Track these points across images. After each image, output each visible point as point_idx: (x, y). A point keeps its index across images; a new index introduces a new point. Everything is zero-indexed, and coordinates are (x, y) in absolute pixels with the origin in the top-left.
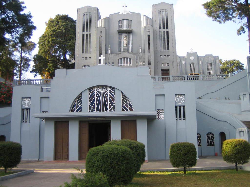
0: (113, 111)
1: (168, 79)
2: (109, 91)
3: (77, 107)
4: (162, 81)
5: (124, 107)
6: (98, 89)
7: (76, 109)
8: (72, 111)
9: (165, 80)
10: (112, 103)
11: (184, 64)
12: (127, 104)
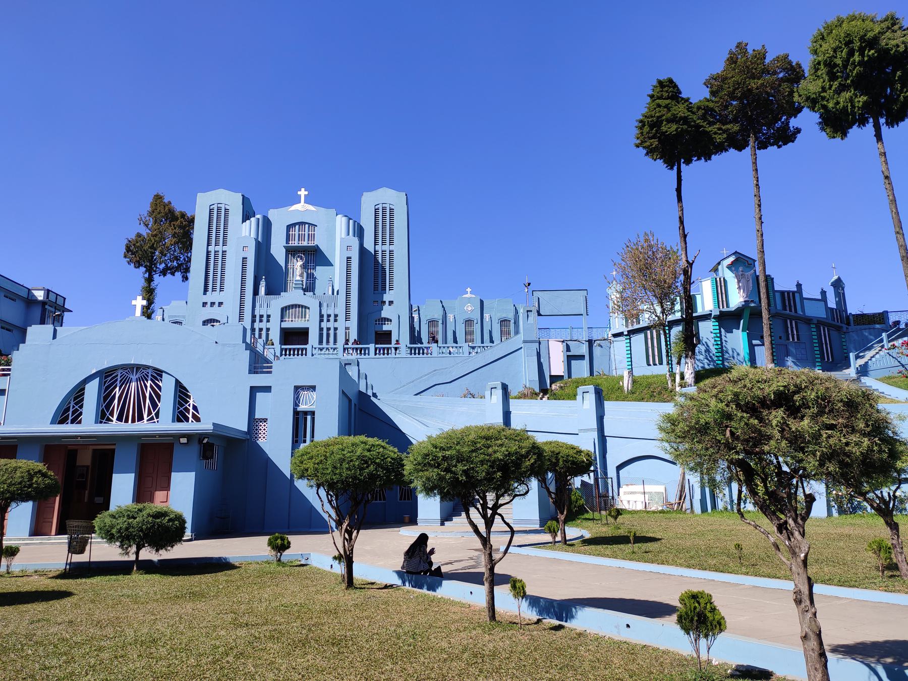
0: (155, 422)
1: (365, 351)
2: (150, 377)
3: (73, 413)
4: (409, 356)
5: (181, 412)
6: (126, 373)
7: (70, 418)
8: (62, 422)
9: (413, 354)
10: (155, 405)
11: (487, 320)
12: (189, 405)
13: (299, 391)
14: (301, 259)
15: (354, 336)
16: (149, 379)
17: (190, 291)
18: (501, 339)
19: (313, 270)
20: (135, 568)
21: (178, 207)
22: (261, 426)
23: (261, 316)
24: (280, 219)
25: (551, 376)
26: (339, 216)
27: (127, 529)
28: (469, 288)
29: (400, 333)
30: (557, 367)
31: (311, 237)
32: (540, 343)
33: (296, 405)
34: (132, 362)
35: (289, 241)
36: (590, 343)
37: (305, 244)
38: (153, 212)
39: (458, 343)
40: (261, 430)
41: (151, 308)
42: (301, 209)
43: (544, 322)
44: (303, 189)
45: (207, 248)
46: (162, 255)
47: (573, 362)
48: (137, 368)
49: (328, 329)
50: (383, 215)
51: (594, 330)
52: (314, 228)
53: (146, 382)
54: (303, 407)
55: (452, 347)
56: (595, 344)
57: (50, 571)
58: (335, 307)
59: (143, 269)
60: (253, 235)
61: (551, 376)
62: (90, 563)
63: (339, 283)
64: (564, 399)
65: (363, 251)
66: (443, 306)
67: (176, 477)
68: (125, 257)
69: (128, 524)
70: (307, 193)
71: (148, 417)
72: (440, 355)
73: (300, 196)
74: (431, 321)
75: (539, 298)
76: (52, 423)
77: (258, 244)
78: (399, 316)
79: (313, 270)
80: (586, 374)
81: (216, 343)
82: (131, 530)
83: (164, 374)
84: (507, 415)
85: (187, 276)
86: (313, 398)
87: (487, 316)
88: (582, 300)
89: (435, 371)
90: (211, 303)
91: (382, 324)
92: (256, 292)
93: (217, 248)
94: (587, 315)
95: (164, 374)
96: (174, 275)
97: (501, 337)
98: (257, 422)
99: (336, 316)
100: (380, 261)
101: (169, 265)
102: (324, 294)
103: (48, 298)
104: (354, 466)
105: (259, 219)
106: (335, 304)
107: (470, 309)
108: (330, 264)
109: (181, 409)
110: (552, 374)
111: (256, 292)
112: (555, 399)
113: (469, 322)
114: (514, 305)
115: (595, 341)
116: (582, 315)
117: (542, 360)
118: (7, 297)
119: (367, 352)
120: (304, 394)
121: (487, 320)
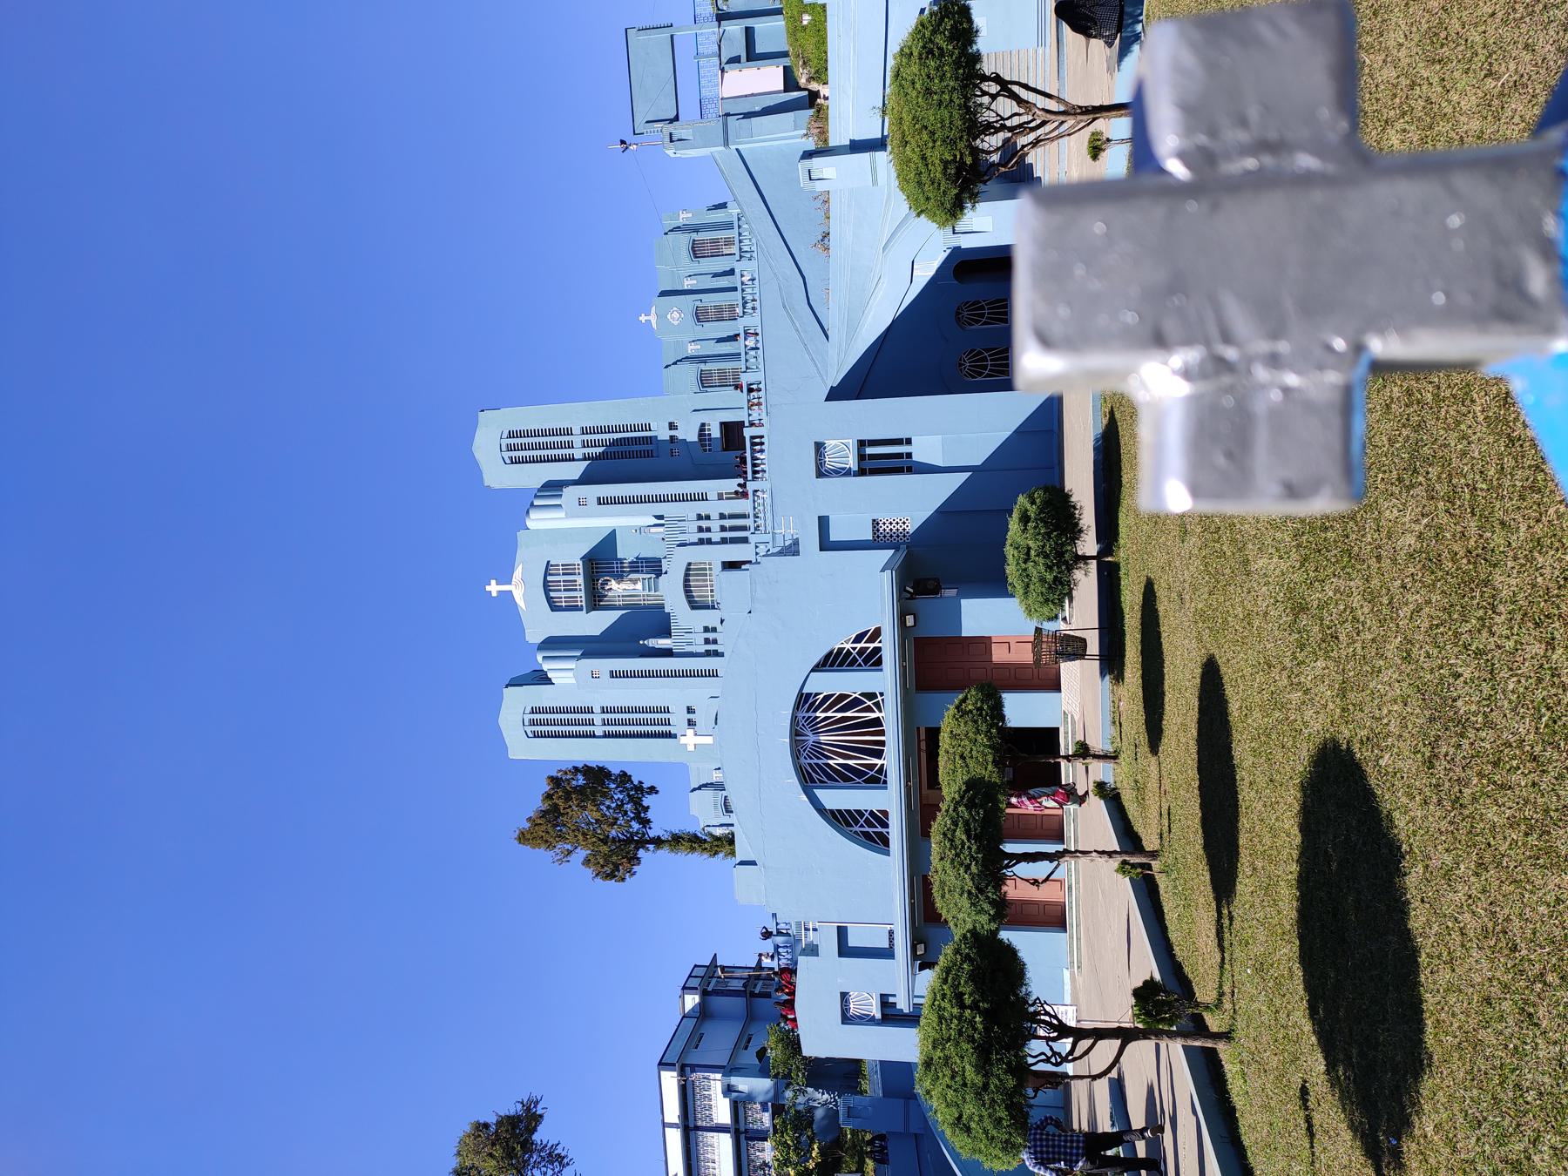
0: (883, 700)
2: (810, 714)
3: (871, 825)
4: (763, 407)
5: (866, 661)
6: (804, 751)
8: (885, 841)
10: (856, 703)
11: (695, 282)
12: (854, 649)
13: (825, 470)
14: (606, 582)
15: (731, 485)
16: (813, 715)
17: (672, 760)
18: (726, 255)
19: (623, 563)
20: (1110, 559)
21: (533, 802)
22: (885, 530)
23: (707, 641)
24: (540, 623)
25: (786, 90)
26: (529, 524)
27: (1046, 556)
28: (640, 318)
29: (727, 406)
30: (769, 79)
31: (568, 569)
32: (728, 115)
33: (848, 473)
34: (788, 740)
35: (578, 606)
36: (722, 17)
37: (580, 580)
38: (547, 841)
39: (737, 333)
40: (891, 530)
41: (704, 837)
42: (522, 589)
43: (689, 110)
44: (488, 588)
45: (599, 737)
46: (615, 823)
47: (759, 49)
48: (796, 735)
49: (723, 529)
50: (523, 446)
51: (698, 12)
52: (552, 566)
53: (818, 720)
54: (851, 462)
55: (742, 276)
56: (725, 8)
57: (1113, 702)
58: (684, 520)
59: (641, 853)
60: (571, 665)
61: (786, 90)
62: (1101, 628)
63: (641, 517)
64: (826, 53)
65: (586, 479)
66: (675, 363)
67: (970, 628)
68: (623, 880)
69: (1038, 555)
70: (493, 582)
71: (875, 712)
72: (761, 366)
73: (499, 592)
74: (702, 384)
75: (647, 122)
76: (888, 854)
77: (585, 655)
78: (694, 411)
79: (623, 563)
80: (779, 23)
81: (750, 612)
82: (1047, 549)
83: (805, 691)
84: (857, 147)
85: (649, 788)
86: (836, 446)
87: (688, 284)
88: (643, 37)
89: (785, 307)
90: (688, 712)
91: (710, 440)
92: (668, 653)
93: (598, 721)
94: (672, 26)
95: (805, 691)
96: (648, 807)
97: (723, 255)
98: (878, 537)
99: (700, 517)
100: (601, 449)
101: (632, 815)
102: (663, 539)
103: (696, 989)
104: (937, 69)
105: (544, 657)
106: (679, 521)
107: (676, 315)
108: (613, 534)
109: (860, 661)
110: (782, 88)
111: (668, 653)
112: (826, 69)
113: (700, 316)
114: (666, 234)
115: (718, 9)
116: (672, 36)
117: (757, 109)
118: (698, 1045)
119: (757, 440)
120: (854, 1009)
121: (695, 282)
